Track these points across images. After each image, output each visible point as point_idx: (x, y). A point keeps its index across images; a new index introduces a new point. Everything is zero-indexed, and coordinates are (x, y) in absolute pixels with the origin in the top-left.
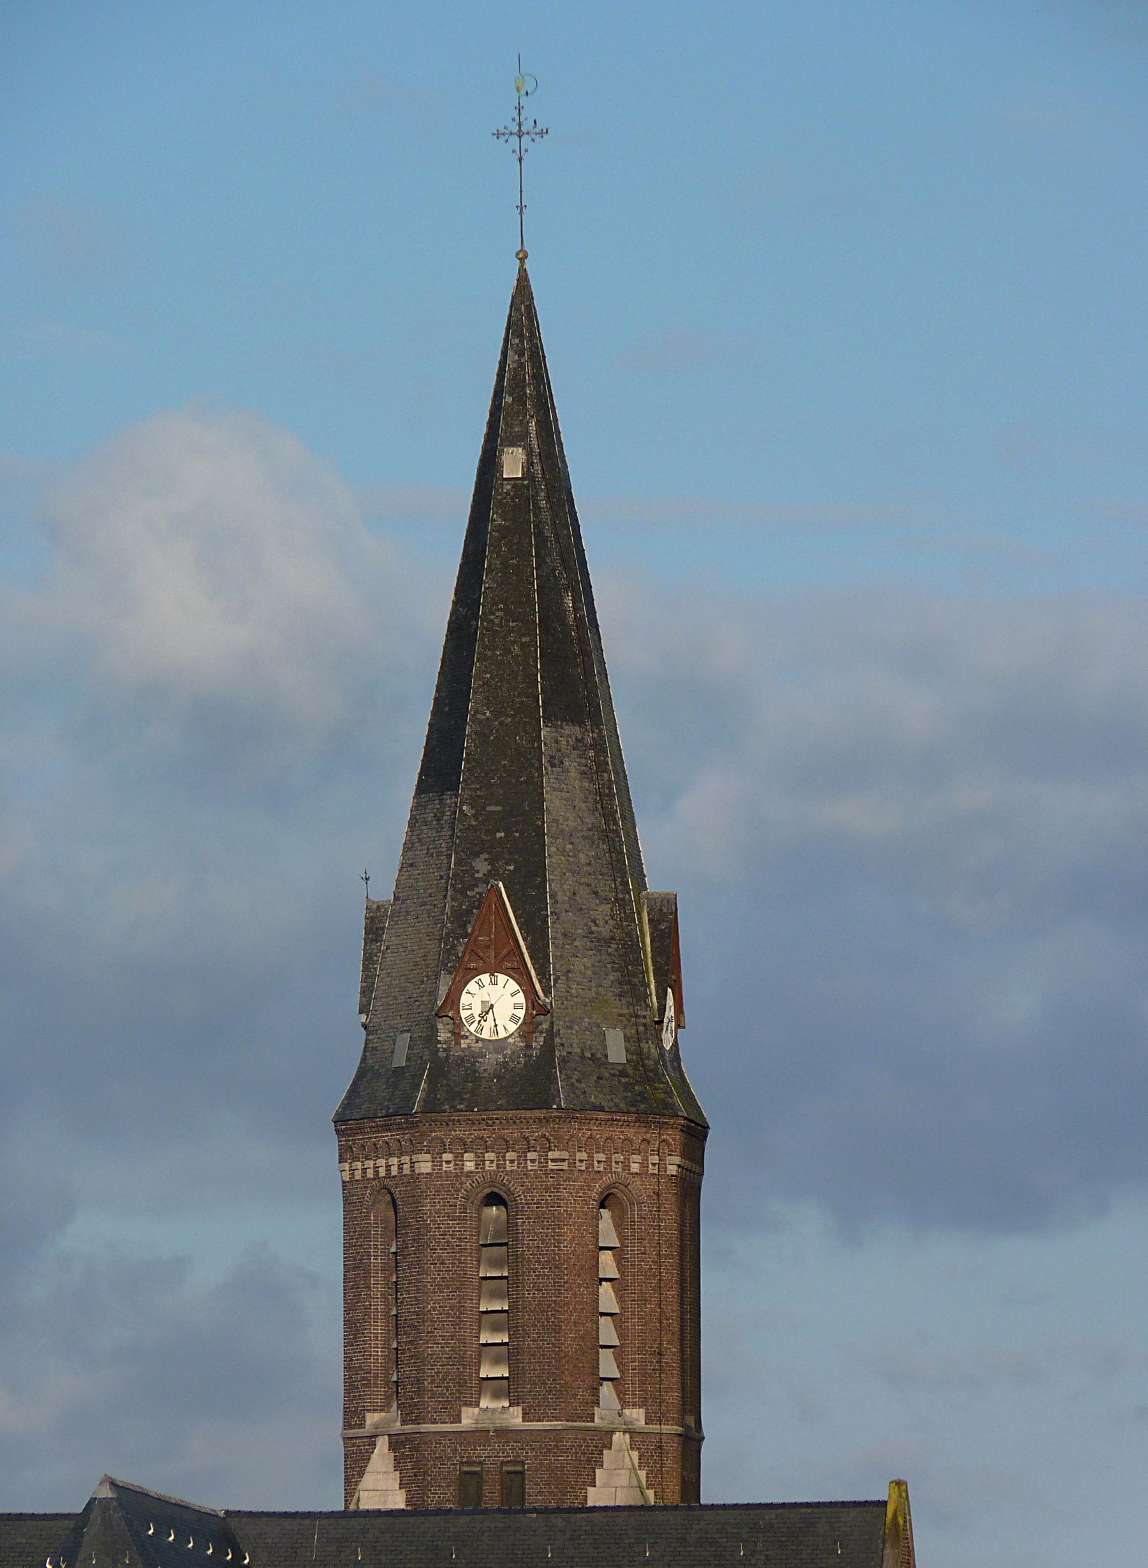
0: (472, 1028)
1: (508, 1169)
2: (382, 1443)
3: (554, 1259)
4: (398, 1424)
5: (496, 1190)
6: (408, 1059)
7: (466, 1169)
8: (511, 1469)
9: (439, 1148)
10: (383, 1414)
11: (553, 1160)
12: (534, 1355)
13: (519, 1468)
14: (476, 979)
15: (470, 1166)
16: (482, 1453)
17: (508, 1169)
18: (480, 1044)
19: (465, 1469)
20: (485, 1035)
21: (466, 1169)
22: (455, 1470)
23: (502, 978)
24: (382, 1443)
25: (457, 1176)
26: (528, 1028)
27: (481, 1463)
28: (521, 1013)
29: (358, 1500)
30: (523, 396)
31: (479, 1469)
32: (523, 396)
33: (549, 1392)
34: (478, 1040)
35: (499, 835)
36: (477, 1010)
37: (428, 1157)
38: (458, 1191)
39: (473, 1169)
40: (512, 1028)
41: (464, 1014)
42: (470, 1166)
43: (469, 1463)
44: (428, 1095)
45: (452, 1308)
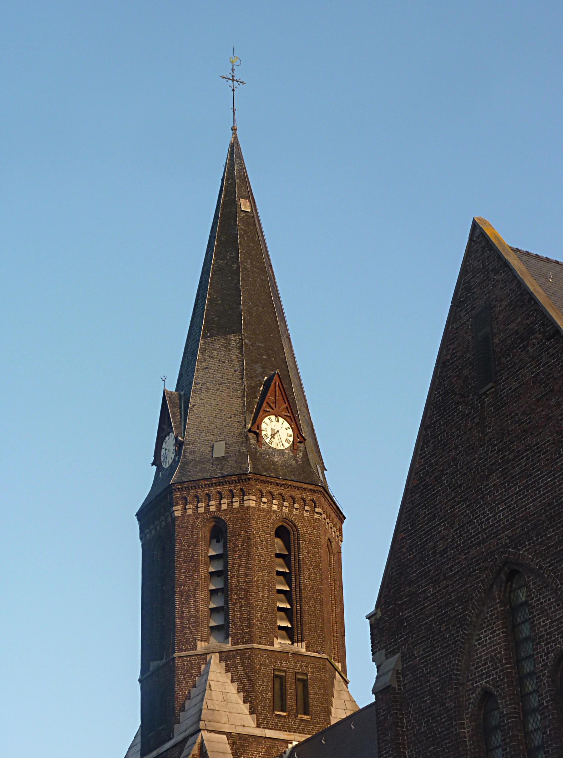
0: (267, 441)
1: (294, 513)
2: (214, 659)
3: (319, 565)
4: (230, 645)
5: (285, 524)
6: (226, 453)
7: (273, 509)
8: (301, 677)
9: (259, 495)
10: (159, 662)
11: (317, 513)
12: (311, 615)
13: (305, 677)
14: (269, 417)
15: (275, 507)
16: (284, 665)
17: (294, 513)
18: (271, 450)
19: (276, 673)
20: (273, 446)
21: (273, 509)
22: (271, 673)
23: (281, 420)
24: (214, 659)
25: (268, 512)
26: (294, 446)
27: (285, 671)
28: (291, 439)
29: (210, 685)
30: (234, 185)
31: (283, 674)
32: (234, 185)
33: (319, 637)
34: (270, 448)
35: (264, 357)
36: (269, 433)
37: (254, 498)
38: (269, 519)
39: (276, 509)
40: (287, 445)
41: (263, 433)
42: (275, 507)
43: (279, 670)
44: (253, 465)
45: (268, 581)
